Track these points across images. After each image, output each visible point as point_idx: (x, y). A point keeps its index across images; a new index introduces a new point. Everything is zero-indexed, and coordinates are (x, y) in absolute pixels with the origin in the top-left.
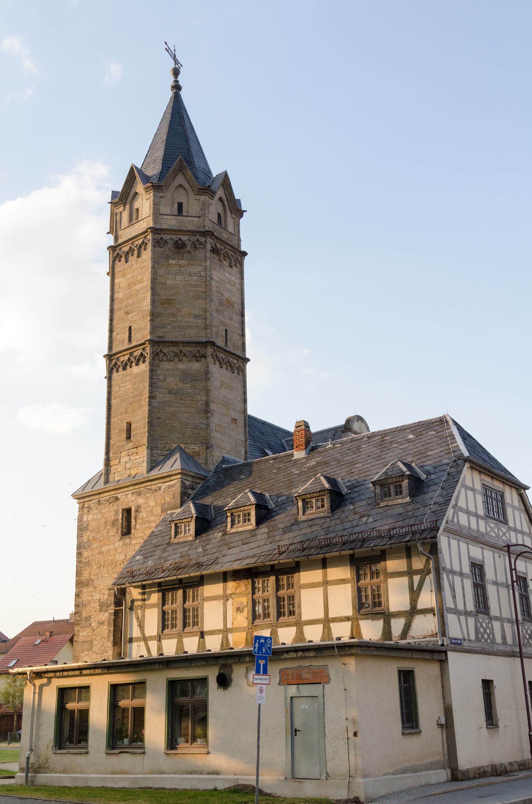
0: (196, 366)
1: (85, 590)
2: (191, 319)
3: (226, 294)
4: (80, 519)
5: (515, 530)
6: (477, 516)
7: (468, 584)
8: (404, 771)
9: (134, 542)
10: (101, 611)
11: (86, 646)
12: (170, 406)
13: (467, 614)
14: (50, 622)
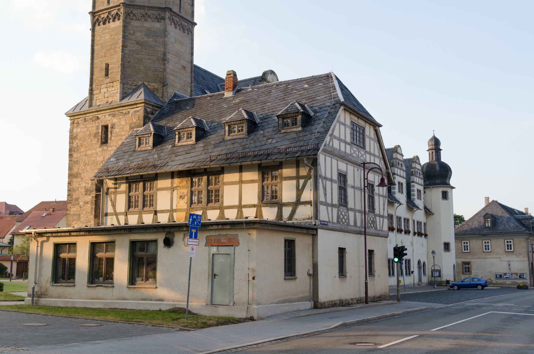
0: (157, 25)
1: (75, 180)
4: (71, 131)
5: (370, 153)
6: (345, 142)
7: (335, 186)
8: (284, 301)
9: (110, 149)
10: (86, 194)
11: (75, 217)
12: (138, 54)
13: (333, 206)
14: (53, 202)
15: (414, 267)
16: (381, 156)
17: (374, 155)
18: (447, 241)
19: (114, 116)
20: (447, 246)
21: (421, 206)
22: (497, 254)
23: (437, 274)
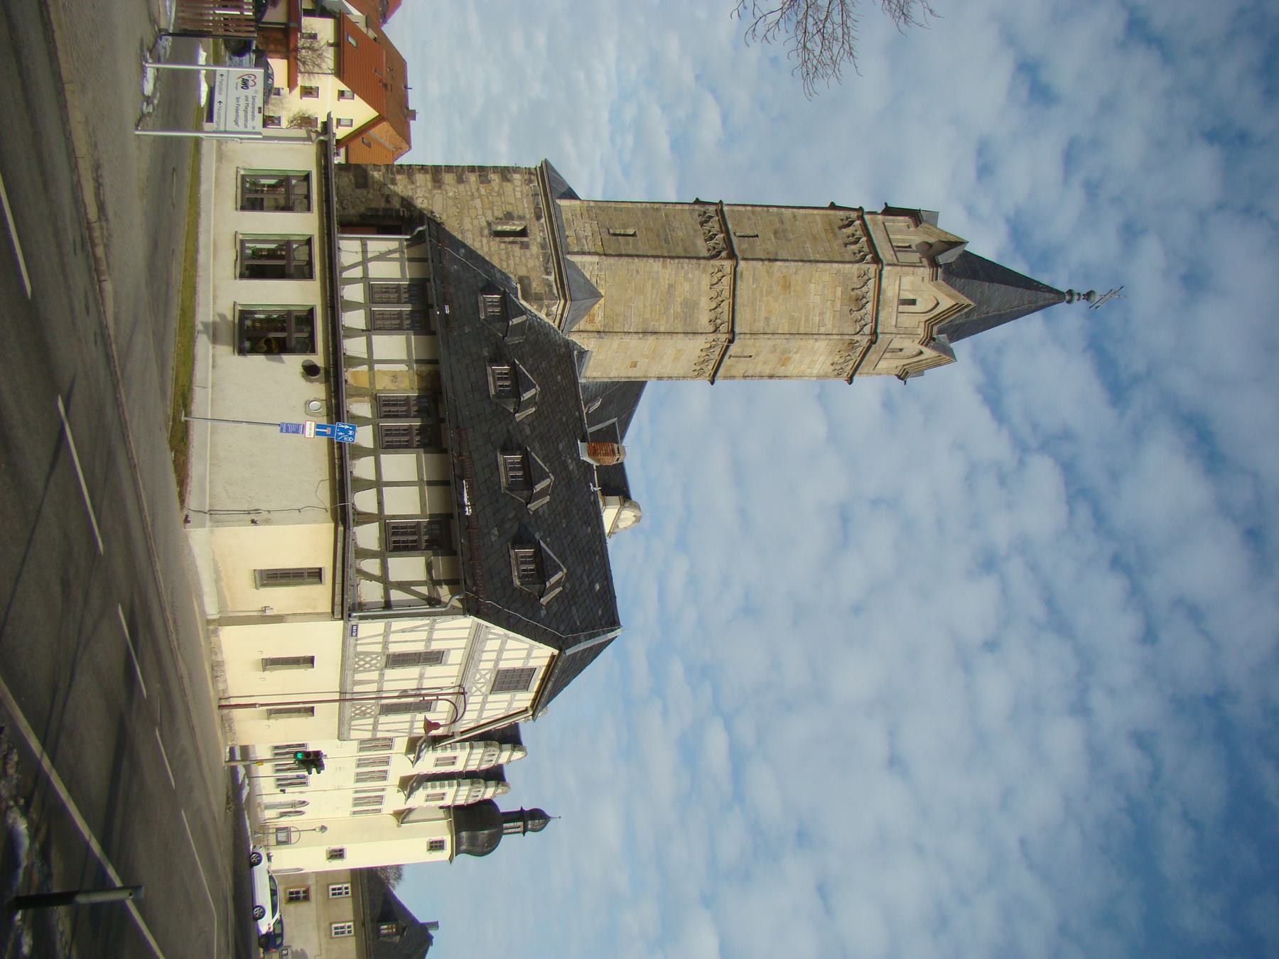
0: (703, 320)
1: (429, 177)
2: (763, 314)
3: (797, 357)
4: (516, 170)
5: (484, 702)
6: (497, 661)
7: (419, 647)
8: (217, 571)
9: (485, 240)
12: (653, 286)
13: (385, 644)
15: (293, 794)
16: (482, 722)
17: (482, 710)
18: (347, 854)
19: (543, 247)
20: (337, 854)
21: (412, 803)
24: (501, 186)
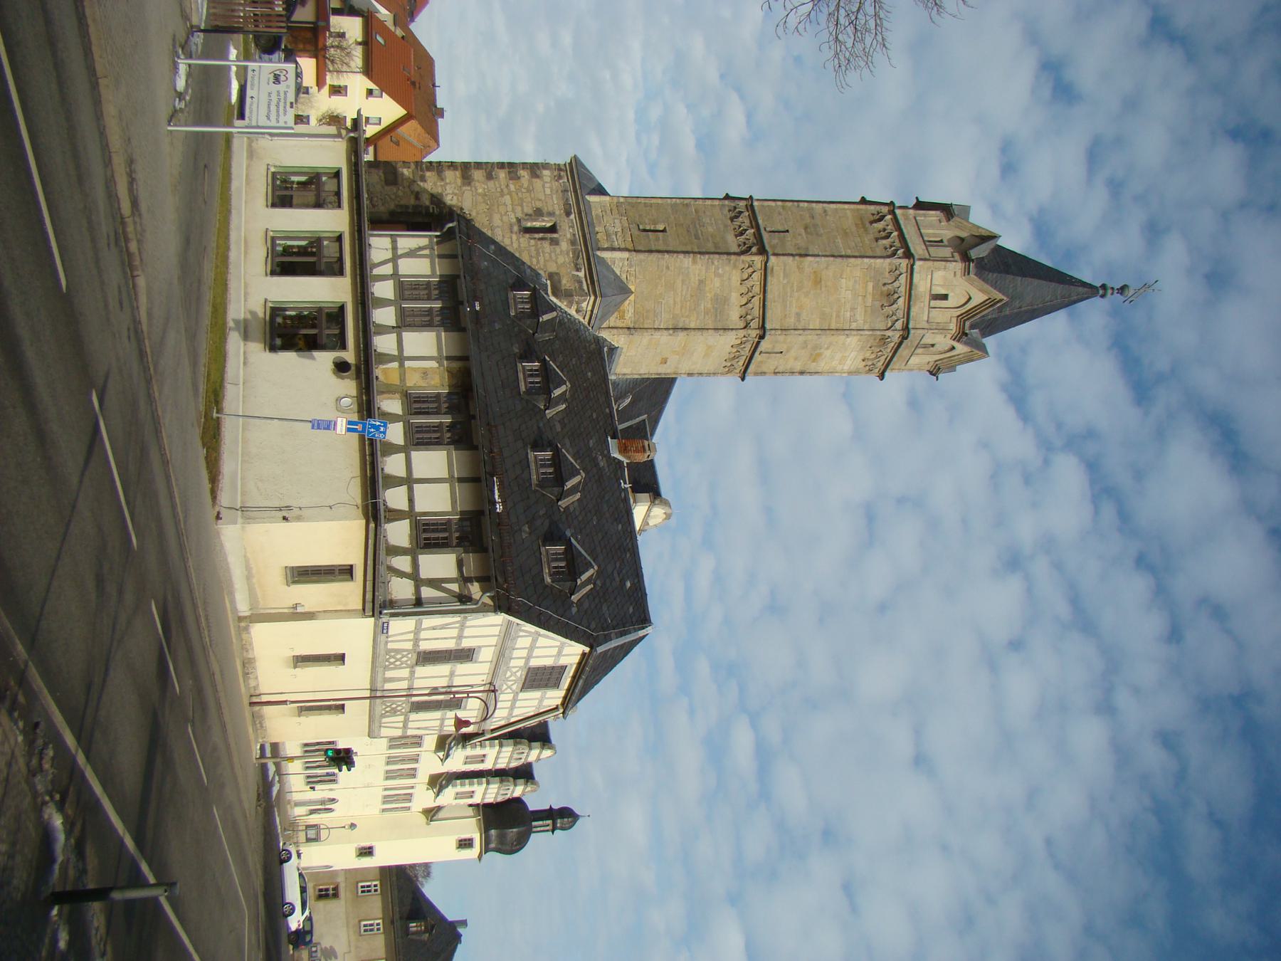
0: (734, 316)
1: (458, 173)
2: (794, 310)
3: (828, 353)
4: (545, 166)
5: (515, 700)
6: (528, 659)
7: (450, 645)
8: (248, 568)
9: (514, 237)
13: (416, 641)
15: (322, 792)
16: (513, 720)
17: (512, 707)
18: (377, 851)
19: (573, 243)
20: (367, 852)
22: (357, 947)
23: (312, 833)
24: (530, 183)
